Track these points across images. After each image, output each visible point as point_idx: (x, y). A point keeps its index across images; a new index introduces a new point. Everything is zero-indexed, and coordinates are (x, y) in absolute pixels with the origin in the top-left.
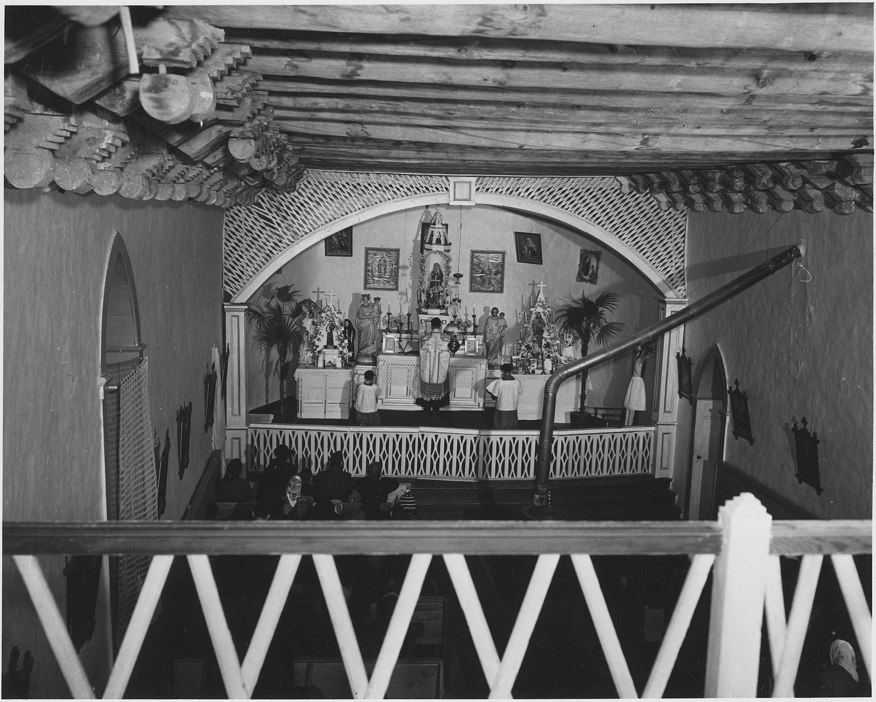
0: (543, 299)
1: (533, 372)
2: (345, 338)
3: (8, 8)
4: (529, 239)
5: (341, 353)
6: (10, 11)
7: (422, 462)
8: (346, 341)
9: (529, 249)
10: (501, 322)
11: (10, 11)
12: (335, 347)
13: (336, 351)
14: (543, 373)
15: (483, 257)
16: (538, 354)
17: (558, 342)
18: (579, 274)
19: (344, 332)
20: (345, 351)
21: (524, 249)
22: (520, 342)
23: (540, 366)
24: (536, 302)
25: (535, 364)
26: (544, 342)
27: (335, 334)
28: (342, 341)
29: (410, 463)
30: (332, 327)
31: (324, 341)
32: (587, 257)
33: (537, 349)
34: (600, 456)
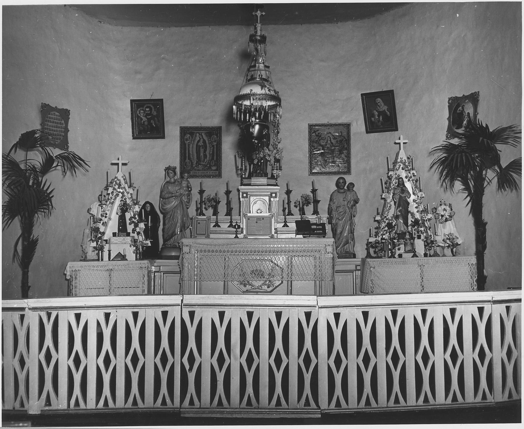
0: (405, 158)
1: (400, 256)
2: (141, 220)
3: (520, 422)
4: (379, 100)
5: (135, 241)
6: (518, 420)
7: (191, 376)
8: (142, 225)
9: (380, 113)
10: (350, 196)
11: (518, 420)
12: (128, 235)
13: (129, 239)
14: (415, 256)
15: (324, 132)
16: (405, 234)
17: (430, 216)
18: (449, 130)
19: (140, 214)
20: (141, 238)
21: (373, 115)
22: (378, 218)
23: (409, 248)
24: (395, 163)
25: (402, 246)
26: (410, 220)
27: (128, 215)
28: (136, 225)
29: (164, 376)
30: (124, 208)
31: (113, 226)
32: (458, 106)
33: (402, 228)
34: (366, 360)
